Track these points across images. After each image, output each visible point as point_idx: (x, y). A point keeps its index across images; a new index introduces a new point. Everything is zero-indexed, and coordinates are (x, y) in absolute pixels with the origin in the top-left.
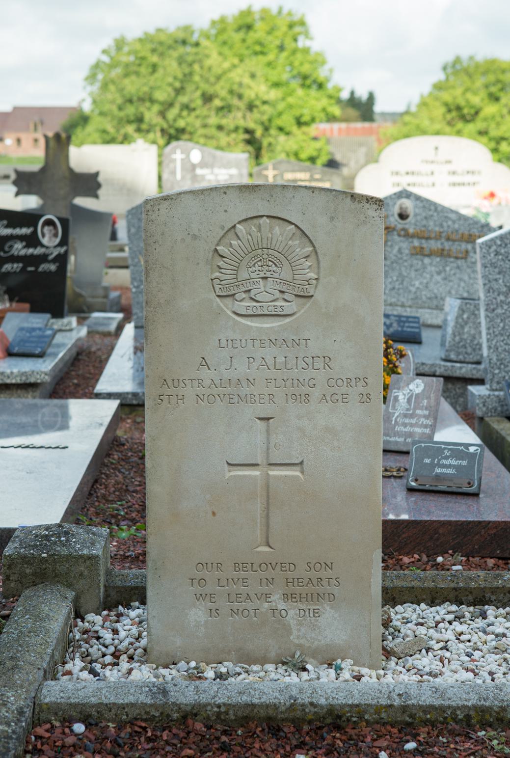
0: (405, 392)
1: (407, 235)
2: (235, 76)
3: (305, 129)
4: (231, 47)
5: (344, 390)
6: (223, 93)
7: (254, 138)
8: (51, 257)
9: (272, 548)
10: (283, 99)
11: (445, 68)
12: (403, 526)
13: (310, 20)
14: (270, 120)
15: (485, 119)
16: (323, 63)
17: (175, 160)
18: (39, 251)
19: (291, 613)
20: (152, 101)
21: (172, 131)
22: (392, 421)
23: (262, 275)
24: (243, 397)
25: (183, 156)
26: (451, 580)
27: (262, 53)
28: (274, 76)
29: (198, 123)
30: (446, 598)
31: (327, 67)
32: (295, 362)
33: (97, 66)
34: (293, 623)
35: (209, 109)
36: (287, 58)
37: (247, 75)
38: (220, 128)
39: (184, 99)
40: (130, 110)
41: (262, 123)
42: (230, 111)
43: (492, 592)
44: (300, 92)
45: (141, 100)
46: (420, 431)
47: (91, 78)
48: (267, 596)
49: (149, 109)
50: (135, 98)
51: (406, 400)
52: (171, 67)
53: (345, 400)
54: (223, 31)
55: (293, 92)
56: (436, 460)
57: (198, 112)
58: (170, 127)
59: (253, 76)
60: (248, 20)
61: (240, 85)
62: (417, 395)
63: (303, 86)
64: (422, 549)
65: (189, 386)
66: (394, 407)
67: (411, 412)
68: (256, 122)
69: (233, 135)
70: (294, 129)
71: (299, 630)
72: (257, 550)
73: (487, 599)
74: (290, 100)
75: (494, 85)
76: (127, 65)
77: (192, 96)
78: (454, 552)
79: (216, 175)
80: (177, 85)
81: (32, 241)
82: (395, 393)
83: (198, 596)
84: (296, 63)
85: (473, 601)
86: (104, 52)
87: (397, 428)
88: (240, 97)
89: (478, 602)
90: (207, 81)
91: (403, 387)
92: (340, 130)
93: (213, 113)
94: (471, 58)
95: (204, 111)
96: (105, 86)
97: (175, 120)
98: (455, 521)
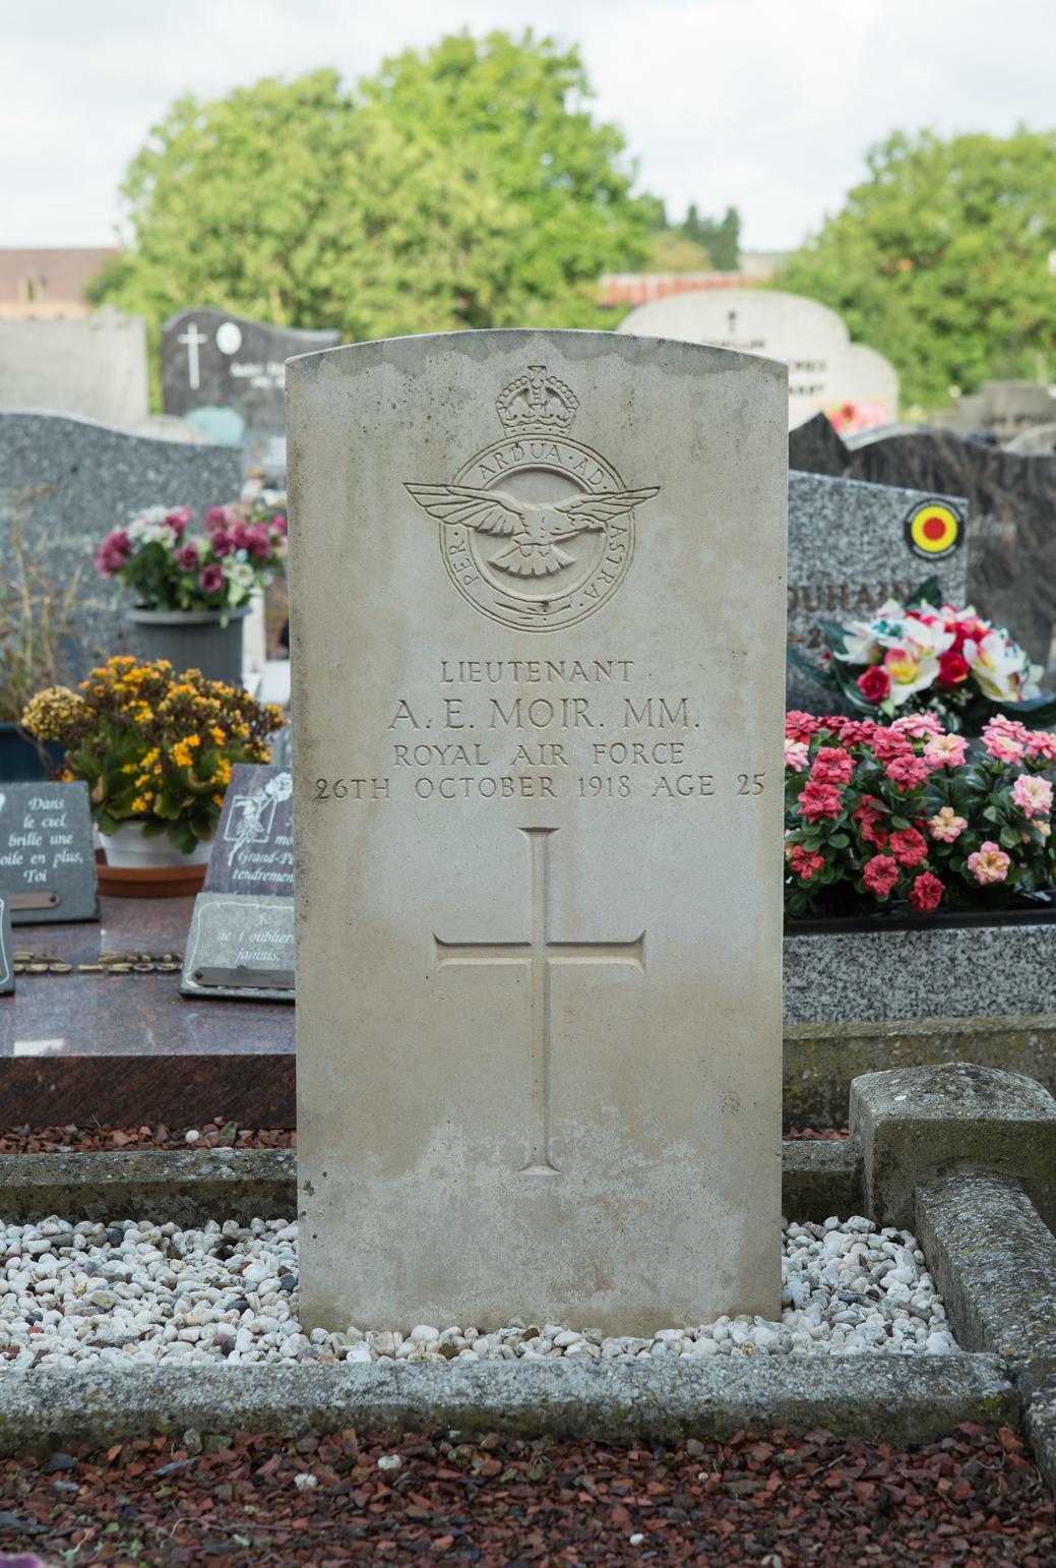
0: (256, 799)
2: (431, 176)
3: (584, 287)
4: (424, 115)
6: (408, 213)
7: (476, 306)
9: (553, 1168)
10: (537, 224)
11: (870, 160)
12: (118, 1068)
13: (590, 57)
14: (508, 269)
15: (959, 262)
16: (619, 145)
17: (186, 346)
20: (261, 232)
21: (303, 295)
22: (227, 859)
25: (203, 339)
26: (65, 1170)
27: (493, 128)
28: (515, 174)
29: (357, 278)
30: (51, 1207)
31: (626, 156)
33: (142, 162)
35: (380, 248)
36: (543, 138)
37: (457, 174)
38: (404, 286)
39: (327, 227)
40: (215, 251)
41: (491, 276)
42: (423, 252)
43: (146, 1192)
44: (572, 209)
45: (239, 229)
46: (281, 880)
47: (132, 188)
49: (254, 248)
50: (224, 227)
51: (258, 816)
52: (298, 161)
54: (406, 81)
55: (556, 208)
56: (242, 934)
57: (356, 255)
58: (299, 284)
59: (470, 177)
60: (462, 55)
61: (444, 195)
62: (281, 805)
63: (577, 195)
64: (161, 1115)
66: (233, 832)
67: (266, 840)
68: (477, 274)
69: (431, 303)
70: (561, 288)
72: (528, 1172)
73: (137, 1207)
74: (551, 226)
75: (978, 190)
76: (206, 156)
77: (342, 221)
78: (225, 1121)
80: (312, 196)
82: (238, 801)
84: (563, 149)
85: (107, 1212)
86: (154, 131)
87: (238, 875)
88: (444, 220)
89: (119, 1213)
90: (373, 188)
91: (254, 789)
93: (388, 256)
94: (925, 134)
95: (365, 252)
96: (163, 200)
97: (309, 272)
98: (227, 1057)
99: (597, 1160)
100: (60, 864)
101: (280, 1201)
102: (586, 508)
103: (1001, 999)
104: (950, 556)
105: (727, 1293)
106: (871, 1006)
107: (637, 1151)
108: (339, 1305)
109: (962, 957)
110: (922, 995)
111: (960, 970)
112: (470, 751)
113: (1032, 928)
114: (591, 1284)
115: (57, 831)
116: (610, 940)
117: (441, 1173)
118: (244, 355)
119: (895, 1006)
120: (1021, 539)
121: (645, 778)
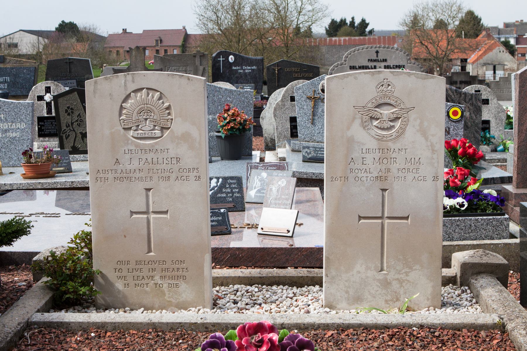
5: (187, 174)
19: (165, 285)
23: (145, 117)
24: (137, 178)
32: (162, 160)
53: (188, 179)
62: (282, 188)
65: (110, 173)
71: (169, 294)
79: (244, 70)
83: (119, 277)
92: (345, 40)
99: (397, 270)
100: (235, 196)
101: (318, 282)
102: (397, 112)
103: (483, 236)
104: (459, 120)
105: (428, 302)
106: (449, 237)
107: (407, 268)
108: (334, 304)
109: (473, 225)
110: (463, 234)
111: (472, 228)
112: (368, 170)
113: (491, 217)
114: (395, 300)
115: (235, 188)
116: (400, 216)
117: (359, 272)
118: (235, 63)
119: (455, 237)
121: (410, 176)
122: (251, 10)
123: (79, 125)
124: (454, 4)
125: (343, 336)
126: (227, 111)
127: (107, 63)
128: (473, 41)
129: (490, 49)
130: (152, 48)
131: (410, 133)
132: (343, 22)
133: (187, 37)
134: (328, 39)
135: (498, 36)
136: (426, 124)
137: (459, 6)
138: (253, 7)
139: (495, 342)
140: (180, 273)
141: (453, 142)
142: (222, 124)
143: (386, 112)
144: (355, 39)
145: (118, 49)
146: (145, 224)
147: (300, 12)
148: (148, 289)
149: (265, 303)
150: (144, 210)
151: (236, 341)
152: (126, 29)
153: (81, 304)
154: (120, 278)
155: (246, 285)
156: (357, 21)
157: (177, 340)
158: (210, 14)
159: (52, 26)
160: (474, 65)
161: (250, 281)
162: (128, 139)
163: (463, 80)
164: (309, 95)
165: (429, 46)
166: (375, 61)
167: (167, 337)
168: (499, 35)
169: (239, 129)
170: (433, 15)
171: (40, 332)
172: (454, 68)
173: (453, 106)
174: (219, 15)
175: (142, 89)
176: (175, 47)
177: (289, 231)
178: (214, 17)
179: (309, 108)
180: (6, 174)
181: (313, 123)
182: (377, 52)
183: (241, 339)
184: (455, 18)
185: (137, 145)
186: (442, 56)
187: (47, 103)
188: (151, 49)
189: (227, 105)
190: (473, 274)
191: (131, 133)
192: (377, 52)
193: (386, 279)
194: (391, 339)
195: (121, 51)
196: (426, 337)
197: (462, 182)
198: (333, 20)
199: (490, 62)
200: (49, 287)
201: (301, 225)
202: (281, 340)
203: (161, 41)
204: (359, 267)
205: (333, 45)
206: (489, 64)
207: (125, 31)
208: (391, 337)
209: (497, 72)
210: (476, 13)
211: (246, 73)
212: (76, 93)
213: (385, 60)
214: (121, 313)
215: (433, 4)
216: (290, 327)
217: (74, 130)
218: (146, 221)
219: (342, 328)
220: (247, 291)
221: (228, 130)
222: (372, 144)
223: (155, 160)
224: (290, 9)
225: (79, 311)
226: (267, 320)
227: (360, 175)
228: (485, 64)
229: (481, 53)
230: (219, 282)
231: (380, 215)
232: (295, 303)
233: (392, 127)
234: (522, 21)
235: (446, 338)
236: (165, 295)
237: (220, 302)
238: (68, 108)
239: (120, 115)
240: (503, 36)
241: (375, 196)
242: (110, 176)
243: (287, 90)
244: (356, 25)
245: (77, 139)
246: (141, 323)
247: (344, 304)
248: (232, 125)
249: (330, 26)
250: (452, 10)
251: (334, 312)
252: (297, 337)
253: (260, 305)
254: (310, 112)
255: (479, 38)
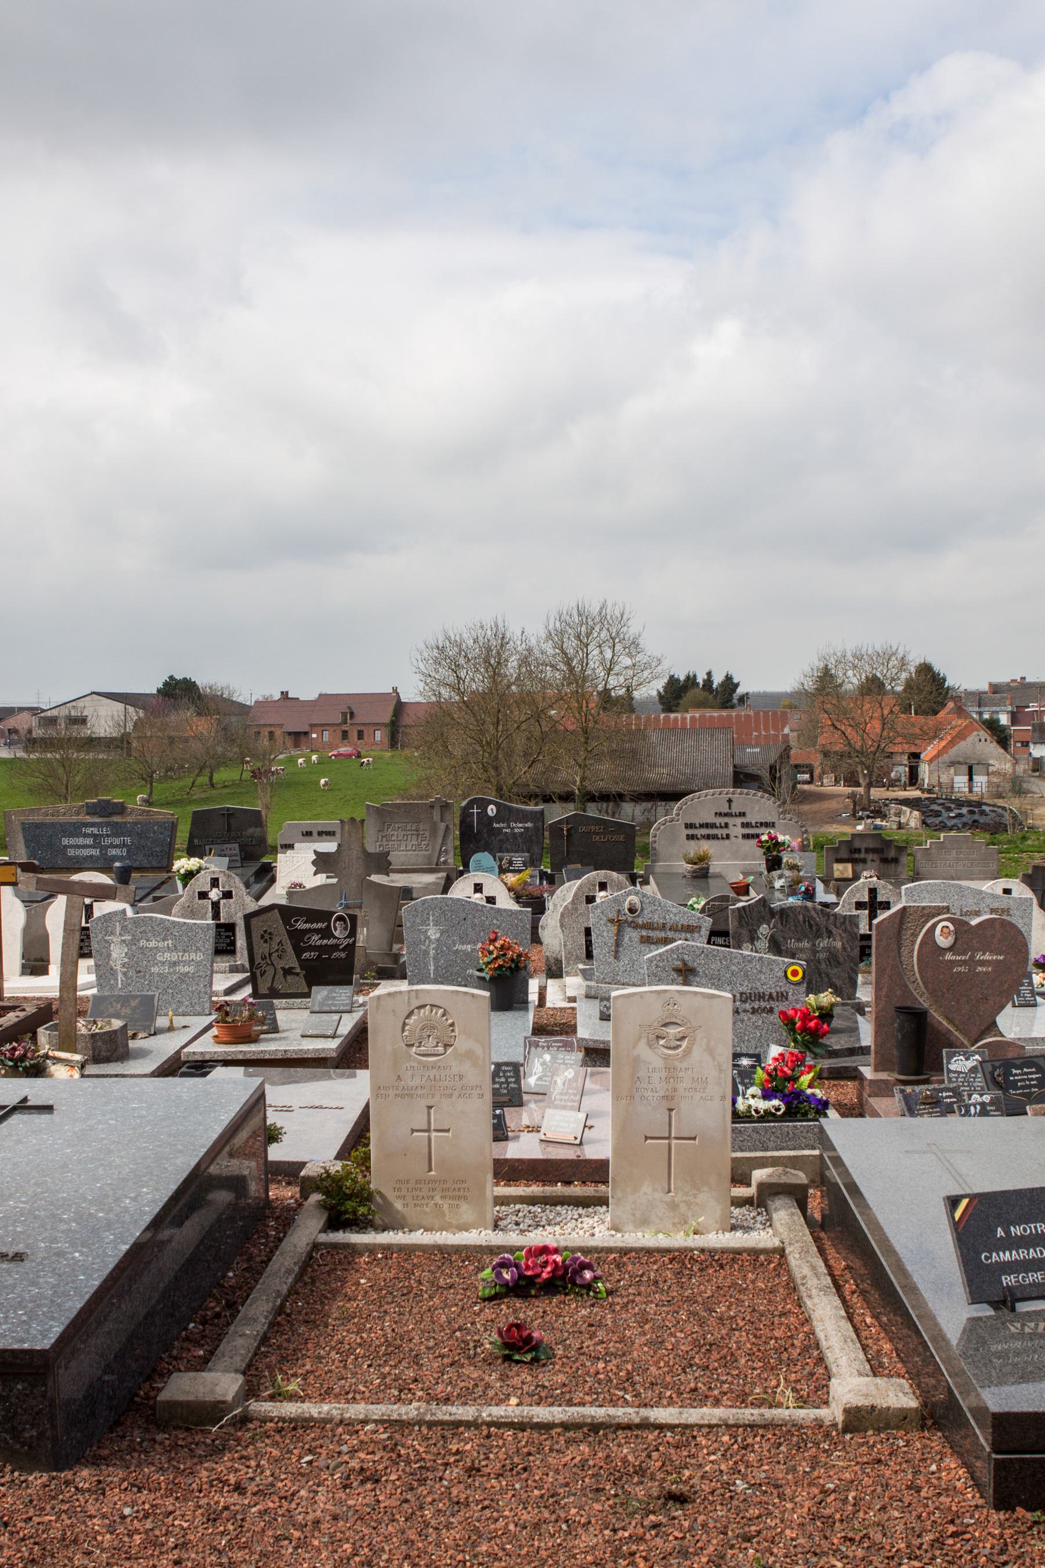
1: (636, 926)
8: (341, 947)
18: (332, 941)
19: (446, 1206)
34: (446, 1211)
48: (433, 1197)
79: (513, 828)
81: (326, 933)
92: (693, 718)
101: (603, 1201)
115: (510, 1077)
117: (646, 1194)
118: (498, 818)
120: (844, 948)
122: (520, 666)
123: (280, 957)
124: (894, 654)
125: (625, 1259)
126: (493, 941)
127: (253, 756)
128: (931, 721)
129: (961, 736)
130: (335, 728)
131: (697, 1053)
132: (691, 681)
133: (400, 707)
134: (662, 716)
135: (977, 709)
136: (712, 1043)
137: (902, 658)
138: (524, 661)
139: (772, 1266)
140: (461, 1193)
141: (791, 1012)
142: (486, 960)
143: (672, 1031)
144: (712, 717)
145: (273, 729)
146: (427, 1143)
147: (610, 669)
148: (427, 1209)
149: (549, 1225)
150: (426, 1127)
151: (523, 1262)
152: (287, 692)
153: (357, 1225)
154: (398, 1197)
155: (528, 1204)
156: (718, 680)
157: (463, 1261)
158: (445, 673)
159: (150, 685)
160: (933, 764)
161: (532, 1201)
162: (411, 1056)
163: (871, 846)
164: (610, 916)
165: (849, 731)
166: (726, 815)
167: (453, 1259)
168: (979, 706)
169: (510, 968)
170: (855, 675)
171: (328, 1252)
172: (895, 769)
173: (793, 964)
174: (463, 674)
175: (425, 1006)
176: (377, 725)
177: (576, 1138)
178: (452, 679)
179: (611, 934)
180: (178, 1029)
181: (616, 957)
182: (730, 801)
183: (527, 1260)
184: (894, 680)
185: (420, 1062)
186: (872, 749)
187: (213, 903)
188: (332, 729)
189: (494, 932)
190: (770, 1195)
191: (414, 1049)
192: (730, 801)
193: (673, 1201)
194: (671, 1263)
195: (278, 733)
196: (706, 1261)
197: (793, 1070)
198: (672, 677)
199: (961, 760)
200: (322, 1206)
201: (591, 1127)
202: (564, 1261)
203: (352, 714)
204: (646, 1188)
205: (672, 728)
206: (959, 763)
207: (285, 695)
208: (671, 1261)
209: (976, 778)
210: (936, 668)
211: (515, 834)
212: (276, 911)
213: (742, 814)
214: (400, 1234)
215: (854, 656)
216: (573, 1250)
217: (272, 964)
218: (427, 1139)
219: (624, 1252)
220: (530, 1212)
221: (495, 969)
222: (658, 1063)
223: (438, 1077)
224: (591, 664)
225: (358, 1232)
226: (551, 1242)
227: (646, 1095)
228: (952, 764)
229: (944, 743)
230: (502, 1201)
231: (667, 1135)
232: (580, 1225)
233: (679, 1046)
234: (1023, 678)
235: (724, 1262)
236: (444, 1215)
237: (502, 1223)
238: (265, 931)
239: (403, 1031)
240: (987, 709)
241: (662, 1116)
242: (392, 1092)
243: (581, 885)
244: (714, 686)
245: (277, 976)
246: (427, 1245)
247: (631, 1227)
248: (500, 962)
249: (665, 688)
250: (890, 666)
251: (619, 1235)
252: (578, 1258)
253: (543, 1226)
254: (613, 941)
255: (942, 714)
